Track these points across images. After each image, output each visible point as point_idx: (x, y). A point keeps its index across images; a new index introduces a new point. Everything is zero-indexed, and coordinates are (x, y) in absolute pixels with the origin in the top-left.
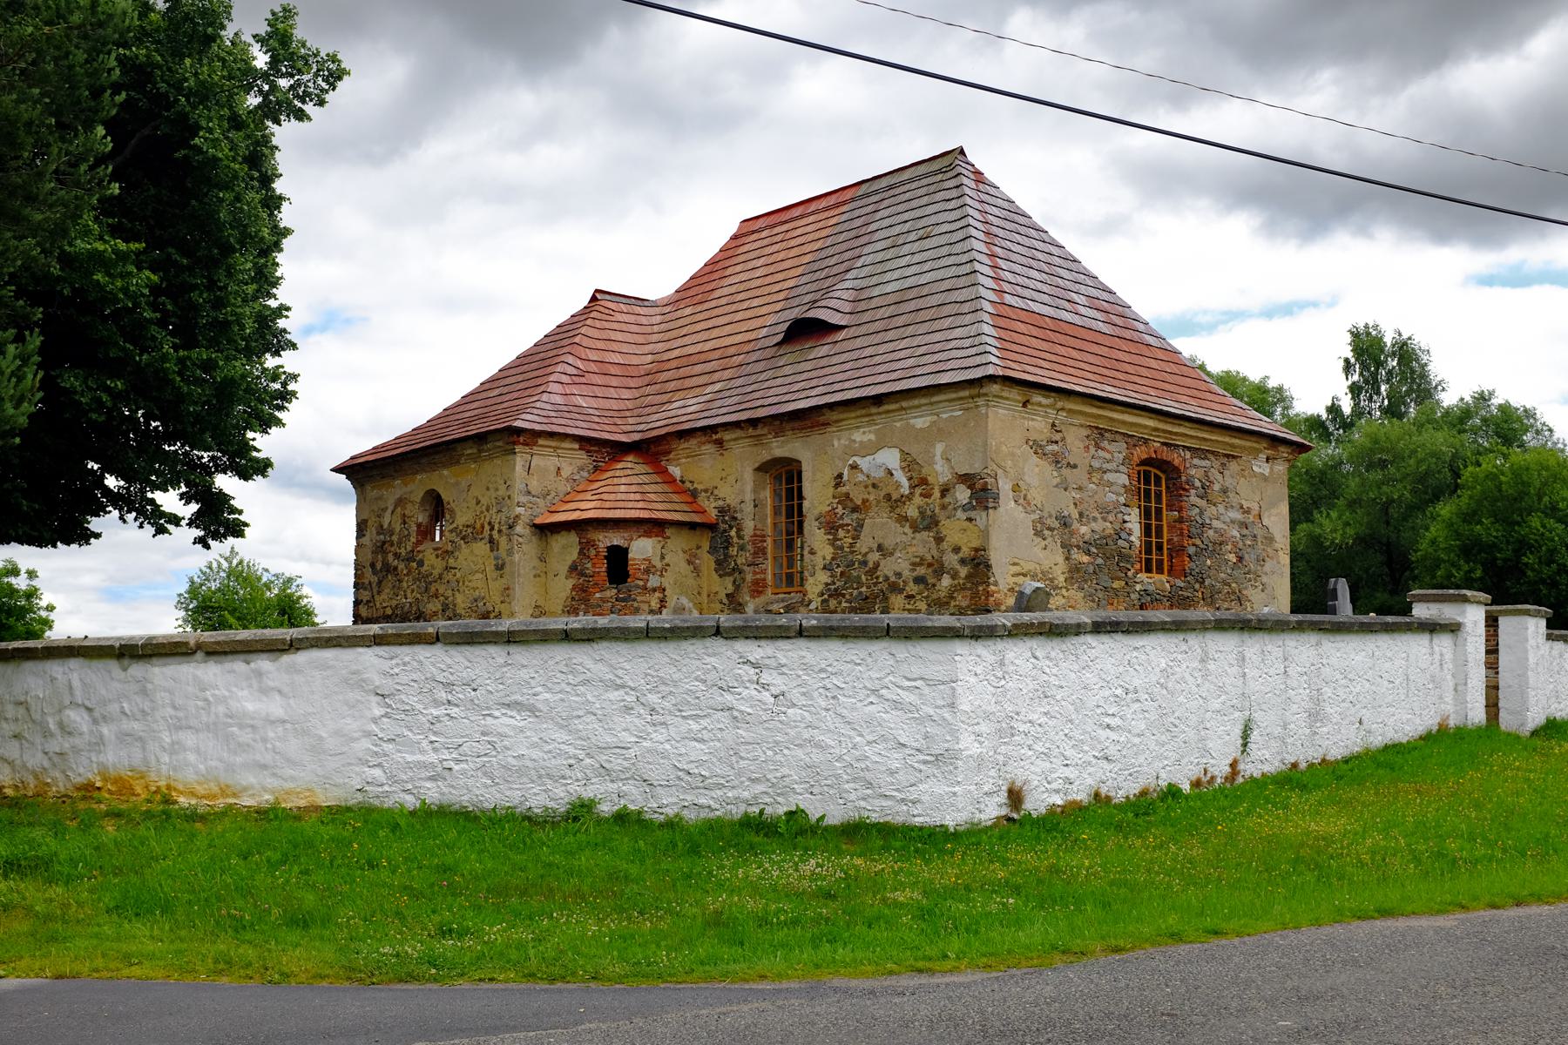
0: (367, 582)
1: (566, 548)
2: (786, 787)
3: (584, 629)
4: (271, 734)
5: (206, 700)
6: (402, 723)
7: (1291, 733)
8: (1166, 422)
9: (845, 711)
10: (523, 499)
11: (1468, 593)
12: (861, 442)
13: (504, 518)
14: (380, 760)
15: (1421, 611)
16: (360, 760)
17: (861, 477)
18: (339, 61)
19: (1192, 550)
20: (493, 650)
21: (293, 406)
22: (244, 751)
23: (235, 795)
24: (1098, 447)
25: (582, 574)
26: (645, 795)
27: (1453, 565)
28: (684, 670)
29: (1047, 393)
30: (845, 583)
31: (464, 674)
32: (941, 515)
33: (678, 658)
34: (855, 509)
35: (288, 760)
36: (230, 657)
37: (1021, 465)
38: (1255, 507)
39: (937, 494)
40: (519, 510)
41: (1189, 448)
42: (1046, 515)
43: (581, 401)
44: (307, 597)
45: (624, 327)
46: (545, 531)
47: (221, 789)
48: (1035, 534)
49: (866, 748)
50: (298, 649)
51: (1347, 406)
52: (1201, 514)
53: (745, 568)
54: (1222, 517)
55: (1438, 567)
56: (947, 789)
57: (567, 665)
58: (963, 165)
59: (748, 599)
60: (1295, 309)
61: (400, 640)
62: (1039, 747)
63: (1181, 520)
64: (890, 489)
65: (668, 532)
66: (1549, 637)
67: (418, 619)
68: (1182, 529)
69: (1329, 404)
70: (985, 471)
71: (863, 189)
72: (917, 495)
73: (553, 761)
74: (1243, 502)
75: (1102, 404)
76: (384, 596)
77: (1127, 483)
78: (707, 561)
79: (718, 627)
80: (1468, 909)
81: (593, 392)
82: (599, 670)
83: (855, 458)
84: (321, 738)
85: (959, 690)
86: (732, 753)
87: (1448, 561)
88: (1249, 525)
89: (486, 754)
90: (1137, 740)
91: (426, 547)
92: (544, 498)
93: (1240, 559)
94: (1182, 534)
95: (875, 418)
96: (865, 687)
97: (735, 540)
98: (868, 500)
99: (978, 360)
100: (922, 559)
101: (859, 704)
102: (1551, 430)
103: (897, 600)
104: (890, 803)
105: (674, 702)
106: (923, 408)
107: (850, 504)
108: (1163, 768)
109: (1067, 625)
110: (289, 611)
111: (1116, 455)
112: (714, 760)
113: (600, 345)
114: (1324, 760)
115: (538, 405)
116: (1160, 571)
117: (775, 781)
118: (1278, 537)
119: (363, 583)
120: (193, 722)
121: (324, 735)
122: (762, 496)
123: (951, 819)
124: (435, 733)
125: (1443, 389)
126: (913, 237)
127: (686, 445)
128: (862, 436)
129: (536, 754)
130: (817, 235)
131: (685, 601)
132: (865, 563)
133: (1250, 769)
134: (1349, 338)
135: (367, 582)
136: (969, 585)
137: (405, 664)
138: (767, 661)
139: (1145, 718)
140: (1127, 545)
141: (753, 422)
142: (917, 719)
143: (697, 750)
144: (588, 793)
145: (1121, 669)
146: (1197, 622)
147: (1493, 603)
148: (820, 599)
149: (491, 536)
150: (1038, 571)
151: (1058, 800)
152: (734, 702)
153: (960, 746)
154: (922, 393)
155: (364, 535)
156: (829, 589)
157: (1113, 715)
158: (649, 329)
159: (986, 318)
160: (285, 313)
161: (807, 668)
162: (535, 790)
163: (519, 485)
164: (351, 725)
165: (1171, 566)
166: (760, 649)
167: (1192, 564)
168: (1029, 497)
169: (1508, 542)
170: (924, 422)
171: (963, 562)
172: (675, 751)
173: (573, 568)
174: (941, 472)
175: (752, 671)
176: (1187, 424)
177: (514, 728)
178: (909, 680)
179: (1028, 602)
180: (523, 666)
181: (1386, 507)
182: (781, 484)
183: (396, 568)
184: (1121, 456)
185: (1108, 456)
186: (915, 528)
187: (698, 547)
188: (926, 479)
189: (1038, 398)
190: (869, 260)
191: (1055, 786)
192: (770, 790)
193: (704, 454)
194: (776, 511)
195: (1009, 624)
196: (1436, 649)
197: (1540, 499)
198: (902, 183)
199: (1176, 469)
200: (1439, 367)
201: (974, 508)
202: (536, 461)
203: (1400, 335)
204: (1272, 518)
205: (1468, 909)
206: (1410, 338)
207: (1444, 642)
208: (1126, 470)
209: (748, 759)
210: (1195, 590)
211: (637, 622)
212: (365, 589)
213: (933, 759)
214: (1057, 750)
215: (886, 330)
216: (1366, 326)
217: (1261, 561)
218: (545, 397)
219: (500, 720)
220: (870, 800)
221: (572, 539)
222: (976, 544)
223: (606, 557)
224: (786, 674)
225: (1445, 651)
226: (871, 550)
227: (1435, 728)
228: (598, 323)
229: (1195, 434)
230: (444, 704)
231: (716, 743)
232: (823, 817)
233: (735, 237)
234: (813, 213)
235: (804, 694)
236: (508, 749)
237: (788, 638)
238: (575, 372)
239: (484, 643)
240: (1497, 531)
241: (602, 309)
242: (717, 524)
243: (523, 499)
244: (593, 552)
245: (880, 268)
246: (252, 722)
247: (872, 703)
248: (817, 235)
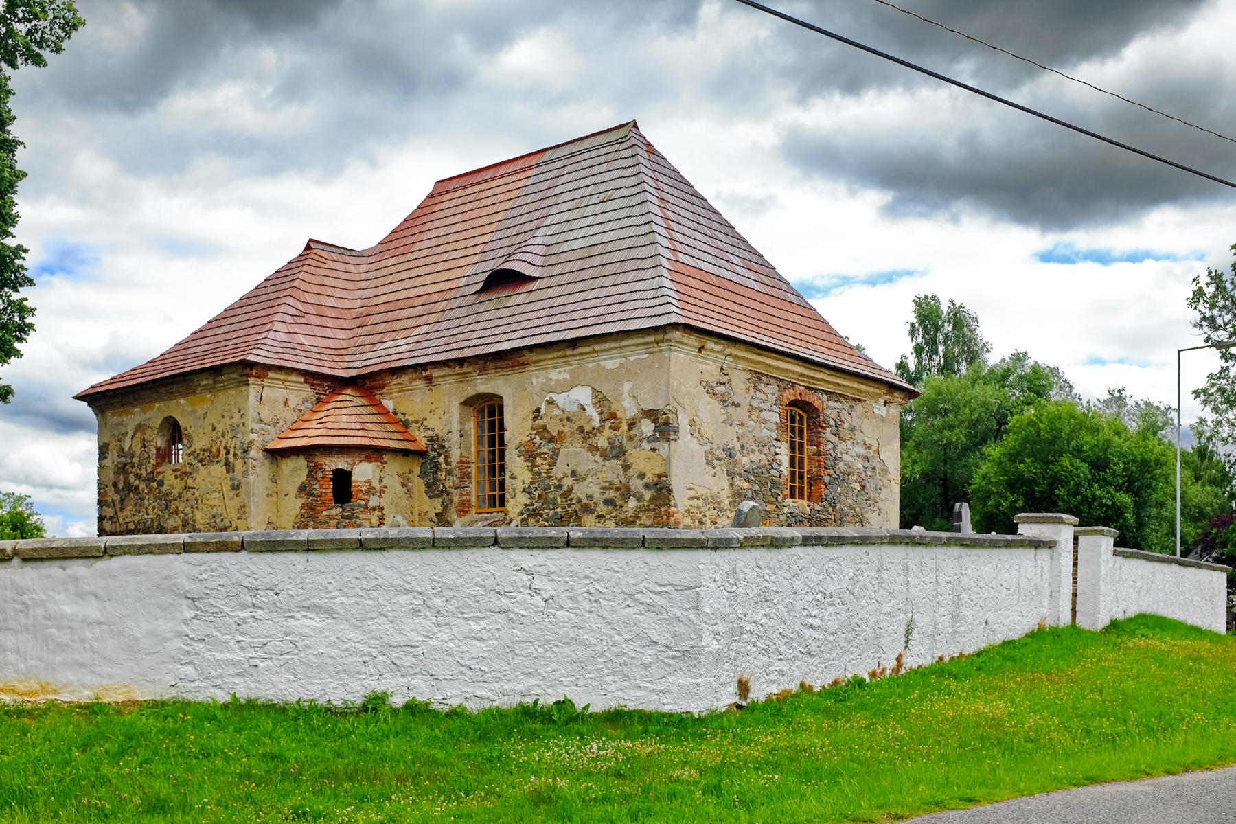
0: (110, 500)
1: (295, 470)
2: (555, 680)
3: (377, 539)
4: (89, 635)
5: (24, 603)
6: (211, 625)
7: (939, 632)
8: (810, 369)
9: (606, 613)
10: (256, 426)
11: (1064, 516)
12: (557, 381)
13: (238, 443)
14: (191, 658)
15: (1026, 530)
16: (173, 658)
17: (557, 412)
18: (75, 11)
19: (827, 479)
20: (292, 557)
21: (32, 337)
22: (63, 651)
23: (55, 692)
24: (756, 389)
25: (310, 494)
26: (431, 688)
27: (1001, 496)
28: (466, 576)
29: (718, 341)
30: (543, 504)
31: (267, 580)
32: (629, 446)
33: (460, 566)
34: (551, 440)
35: (105, 659)
36: (46, 563)
37: (696, 403)
38: (875, 444)
39: (624, 427)
40: (253, 436)
41: (826, 392)
42: (715, 447)
43: (302, 339)
44: (37, 514)
45: (336, 274)
46: (276, 455)
47: (41, 686)
48: (707, 463)
49: (624, 645)
50: (112, 556)
51: (912, 364)
52: (834, 448)
53: (453, 490)
54: (850, 452)
55: (989, 497)
56: (692, 681)
57: (360, 572)
58: (637, 137)
59: (455, 517)
60: (894, 277)
61: (208, 548)
62: (761, 644)
63: (819, 454)
64: (583, 423)
65: (386, 458)
66: (1115, 554)
67: (160, 532)
68: (819, 461)
69: (899, 362)
70: (668, 407)
71: (548, 156)
72: (607, 428)
73: (350, 659)
74: (866, 439)
75: (761, 352)
76: (126, 512)
77: (778, 421)
78: (418, 484)
79: (496, 539)
80: (1152, 775)
81: (313, 332)
82: (390, 576)
83: (551, 395)
84: (136, 639)
85: (703, 595)
86: (508, 650)
87: (997, 493)
88: (870, 459)
89: (288, 653)
90: (831, 638)
91: (165, 468)
92: (275, 426)
93: (863, 487)
94: (819, 466)
95: (570, 359)
96: (623, 592)
97: (443, 466)
98: (562, 432)
99: (662, 310)
100: (611, 484)
101: (618, 607)
102: (1071, 387)
103: (589, 520)
104: (643, 693)
105: (456, 605)
106: (614, 351)
107: (546, 435)
108: (850, 662)
109: (784, 538)
110: (20, 527)
111: (770, 396)
112: (493, 656)
113: (316, 289)
114: (961, 655)
115: (266, 341)
116: (801, 497)
117: (545, 674)
118: (891, 469)
119: (106, 501)
120: (12, 624)
121: (140, 635)
122: (467, 427)
123: (696, 707)
124: (242, 634)
125: (988, 351)
126: (595, 199)
127: (398, 381)
128: (558, 374)
129: (334, 652)
130: (507, 196)
131: (399, 519)
132: (560, 487)
133: (911, 662)
134: (913, 307)
135: (110, 500)
136: (652, 507)
137: (212, 571)
138: (539, 569)
139: (838, 619)
140: (778, 474)
141: (460, 362)
142: (667, 620)
143: (477, 648)
144: (380, 689)
145: (821, 577)
146: (877, 537)
147: (1080, 525)
148: (520, 518)
149: (227, 459)
150: (709, 495)
151: (775, 690)
152: (510, 605)
153: (703, 643)
154: (613, 337)
155: (106, 458)
156: (528, 510)
157: (815, 616)
158: (357, 277)
159: (665, 273)
160: (23, 255)
161: (573, 574)
162: (333, 685)
163: (252, 414)
164: (164, 626)
165: (810, 493)
166: (532, 558)
167: (827, 491)
168: (702, 431)
169: (1044, 478)
170: (614, 364)
171: (647, 486)
172: (458, 649)
173: (302, 489)
174: (628, 408)
175: (525, 578)
176: (826, 371)
177: (314, 628)
178: (660, 585)
179: (746, 518)
180: (322, 573)
181: (945, 447)
182: (483, 417)
183: (137, 488)
184: (774, 398)
185: (764, 397)
186: (605, 457)
187: (411, 472)
188: (615, 414)
189: (711, 345)
190: (556, 219)
191: (772, 677)
192: (541, 682)
193: (415, 389)
194: (479, 441)
195: (742, 537)
196: (1039, 562)
197: (1069, 443)
198: (583, 152)
199: (816, 410)
200: (986, 331)
201: (657, 440)
202: (267, 391)
203: (954, 304)
204: (887, 454)
205: (1152, 775)
206: (961, 307)
207: (1044, 554)
208: (778, 410)
209: (522, 656)
210: (829, 514)
211: (351, 534)
212: (108, 506)
213: (680, 654)
214: (774, 647)
215: (575, 282)
216: (926, 297)
217: (878, 489)
218: (271, 335)
219: (301, 622)
220: (627, 691)
221: (301, 462)
222: (659, 471)
223: (331, 480)
224: (555, 580)
225: (1044, 564)
226: (566, 476)
227: (1036, 627)
228: (313, 270)
229: (832, 380)
230: (249, 607)
231: (494, 642)
232: (588, 706)
233: (431, 196)
234: (502, 176)
235: (570, 598)
236: (309, 647)
237: (557, 548)
238: (296, 313)
239: (285, 551)
240: (1036, 468)
241: (316, 257)
242: (427, 451)
243: (256, 426)
244: (320, 475)
245: (566, 227)
246: (70, 624)
247: (629, 606)
248: (507, 196)
